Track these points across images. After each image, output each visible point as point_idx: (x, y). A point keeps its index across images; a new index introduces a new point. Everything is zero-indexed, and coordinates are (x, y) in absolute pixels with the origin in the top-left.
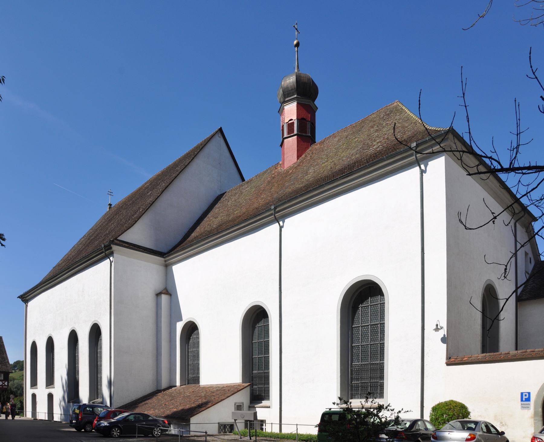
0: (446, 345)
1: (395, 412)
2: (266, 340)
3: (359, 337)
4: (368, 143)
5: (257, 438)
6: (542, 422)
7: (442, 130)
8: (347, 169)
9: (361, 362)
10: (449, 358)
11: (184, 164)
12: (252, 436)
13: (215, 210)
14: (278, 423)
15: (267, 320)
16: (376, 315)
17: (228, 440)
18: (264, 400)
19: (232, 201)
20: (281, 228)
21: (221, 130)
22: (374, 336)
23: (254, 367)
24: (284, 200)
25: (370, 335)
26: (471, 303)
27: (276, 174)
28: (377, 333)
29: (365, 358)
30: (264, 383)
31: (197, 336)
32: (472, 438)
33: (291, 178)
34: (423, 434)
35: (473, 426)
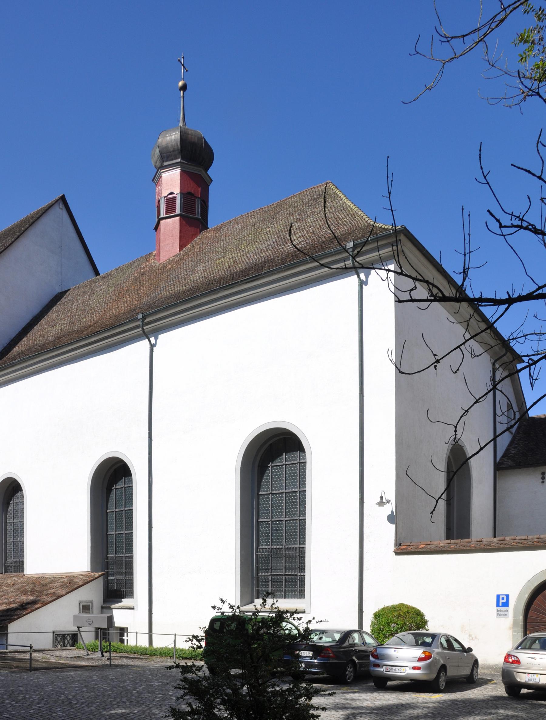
0: (394, 525)
1: (303, 622)
2: (129, 508)
3: (269, 509)
4: (285, 236)
5: (112, 655)
6: (523, 634)
7: (391, 229)
8: (252, 271)
9: (272, 545)
10: (398, 544)
11: (3, 244)
12: (106, 652)
13: (52, 314)
14: (147, 631)
15: (129, 479)
16: (293, 479)
17: (68, 657)
18: (125, 598)
19: (78, 303)
20: (152, 346)
21: (63, 199)
22: (291, 508)
23: (109, 548)
24: (158, 307)
25: (284, 507)
26: (407, 474)
27: (147, 269)
28: (295, 505)
29: (278, 539)
30: (125, 572)
31: (21, 501)
32: (427, 657)
33: (169, 275)
34: (360, 651)
35: (429, 640)
